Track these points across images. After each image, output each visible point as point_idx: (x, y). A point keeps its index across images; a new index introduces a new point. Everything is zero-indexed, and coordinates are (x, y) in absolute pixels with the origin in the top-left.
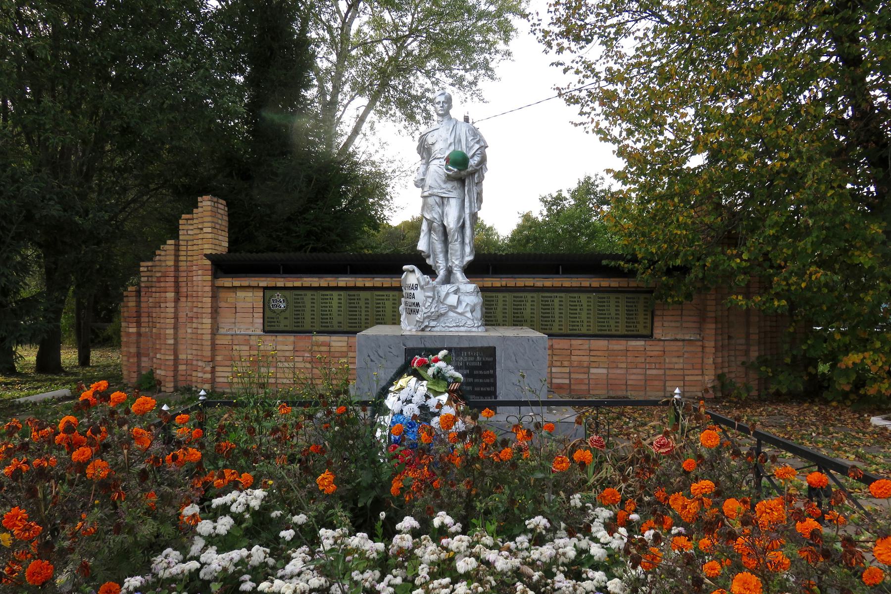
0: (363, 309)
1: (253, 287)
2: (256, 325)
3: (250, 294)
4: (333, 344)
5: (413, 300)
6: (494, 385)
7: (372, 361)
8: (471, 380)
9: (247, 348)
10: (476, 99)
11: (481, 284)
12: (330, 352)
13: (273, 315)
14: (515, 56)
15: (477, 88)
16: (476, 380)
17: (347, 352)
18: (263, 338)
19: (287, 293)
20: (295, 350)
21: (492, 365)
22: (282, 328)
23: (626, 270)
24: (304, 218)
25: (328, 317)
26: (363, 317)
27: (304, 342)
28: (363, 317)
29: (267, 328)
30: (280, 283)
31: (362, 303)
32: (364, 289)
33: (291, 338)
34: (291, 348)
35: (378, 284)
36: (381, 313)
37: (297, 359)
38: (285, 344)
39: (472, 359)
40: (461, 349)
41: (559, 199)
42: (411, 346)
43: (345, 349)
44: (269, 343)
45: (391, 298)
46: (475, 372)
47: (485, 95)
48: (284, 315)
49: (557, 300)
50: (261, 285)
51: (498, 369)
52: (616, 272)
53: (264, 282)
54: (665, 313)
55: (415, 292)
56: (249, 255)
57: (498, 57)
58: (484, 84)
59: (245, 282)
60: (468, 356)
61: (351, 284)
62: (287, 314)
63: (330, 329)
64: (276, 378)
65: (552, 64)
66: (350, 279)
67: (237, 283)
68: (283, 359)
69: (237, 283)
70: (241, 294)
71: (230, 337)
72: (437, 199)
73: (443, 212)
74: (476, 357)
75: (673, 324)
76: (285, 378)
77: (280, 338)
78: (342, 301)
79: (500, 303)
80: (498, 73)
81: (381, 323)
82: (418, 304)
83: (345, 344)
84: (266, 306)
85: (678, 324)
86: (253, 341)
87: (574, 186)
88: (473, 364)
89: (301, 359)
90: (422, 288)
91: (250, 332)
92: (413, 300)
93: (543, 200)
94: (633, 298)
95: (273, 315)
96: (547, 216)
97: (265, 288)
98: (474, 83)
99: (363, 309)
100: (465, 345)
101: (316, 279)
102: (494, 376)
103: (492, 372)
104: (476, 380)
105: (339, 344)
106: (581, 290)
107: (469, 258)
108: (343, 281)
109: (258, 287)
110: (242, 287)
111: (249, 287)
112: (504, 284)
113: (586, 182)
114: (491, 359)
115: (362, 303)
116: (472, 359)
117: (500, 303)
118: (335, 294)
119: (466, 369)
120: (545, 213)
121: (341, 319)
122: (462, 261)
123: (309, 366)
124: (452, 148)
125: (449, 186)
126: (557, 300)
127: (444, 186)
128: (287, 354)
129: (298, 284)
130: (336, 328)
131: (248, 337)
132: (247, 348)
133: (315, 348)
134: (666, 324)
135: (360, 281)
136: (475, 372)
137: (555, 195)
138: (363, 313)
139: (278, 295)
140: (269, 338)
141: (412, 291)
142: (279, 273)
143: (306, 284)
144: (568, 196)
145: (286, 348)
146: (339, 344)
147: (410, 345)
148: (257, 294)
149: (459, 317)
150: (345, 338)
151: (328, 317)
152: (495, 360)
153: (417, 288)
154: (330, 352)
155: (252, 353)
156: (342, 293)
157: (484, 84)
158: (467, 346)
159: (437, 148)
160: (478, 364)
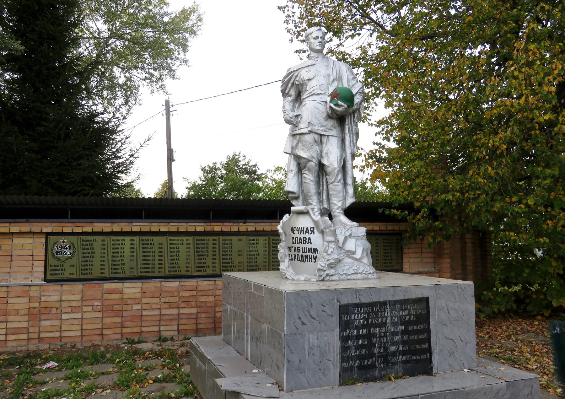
0: (157, 254)
1: (34, 233)
2: (36, 274)
3: (31, 241)
4: (126, 291)
5: (308, 246)
6: (428, 340)
7: (303, 324)
8: (406, 337)
9: (26, 300)
10: (161, 91)
11: (370, 228)
12: (122, 299)
13: (57, 263)
14: (190, 63)
15: (163, 83)
16: (412, 337)
17: (141, 299)
18: (45, 288)
19: (74, 239)
20: (83, 299)
21: (425, 318)
22: (67, 276)
23: (400, 218)
24: (79, 165)
25: (120, 263)
26: (157, 262)
27: (93, 289)
28: (157, 262)
29: (49, 277)
30: (68, 228)
31: (156, 248)
32: (160, 233)
33: (79, 287)
34: (79, 297)
35: (174, 229)
36: (175, 258)
37: (85, 309)
38: (72, 293)
39: (406, 312)
40: (395, 302)
41: (213, 169)
42: (346, 302)
43: (139, 296)
44: (53, 294)
45: (185, 242)
46: (411, 328)
47: (168, 89)
48: (69, 262)
49: (211, 242)
50: (45, 230)
51: (432, 323)
52: (392, 219)
53: (48, 227)
54: (411, 251)
55: (312, 236)
56: (35, 198)
57: (177, 63)
58: (168, 81)
59: (26, 227)
60: (402, 310)
61: (146, 229)
62: (73, 261)
63: (120, 275)
64: (61, 331)
65: (297, 51)
66: (145, 224)
67: (15, 228)
68: (69, 310)
69: (15, 228)
70: (18, 241)
71: (5, 289)
72: (317, 137)
73: (321, 151)
74: (410, 310)
75: (416, 260)
76: (72, 332)
77: (66, 287)
78: (135, 246)
79: (211, 246)
80: (177, 74)
81: (256, 270)
82: (316, 250)
83: (139, 290)
84: (49, 254)
85: (420, 260)
86: (34, 292)
87: (224, 161)
88: (408, 318)
89: (90, 309)
90: (322, 232)
91: (29, 283)
92: (308, 246)
93: (203, 170)
94: (389, 239)
95: (57, 263)
96: (204, 181)
97: (48, 234)
98: (161, 78)
99: (157, 254)
100: (400, 297)
101: (109, 224)
102: (428, 331)
103: (425, 325)
104: (412, 337)
105: (134, 290)
106: (256, 233)
107: (350, 201)
108: (137, 226)
109: (41, 233)
110: (20, 233)
111: (31, 233)
112: (383, 228)
113: (234, 158)
114: (424, 312)
115: (156, 248)
116: (406, 312)
117: (211, 246)
118: (127, 239)
119: (401, 324)
120: (203, 178)
121: (133, 264)
122: (344, 203)
123: (99, 315)
124: (335, 84)
125: (330, 123)
126: (211, 242)
127: (324, 123)
128: (74, 304)
129: (88, 229)
130: (128, 274)
131: (27, 288)
132: (26, 300)
133: (105, 296)
134: (411, 260)
135: (155, 226)
136: (411, 328)
137: (211, 165)
138: (157, 258)
139: (64, 242)
140: (54, 288)
141: (307, 236)
142: (66, 217)
143: (97, 229)
144: (220, 167)
145: (73, 298)
146: (134, 290)
147: (346, 300)
148: (37, 240)
149: (356, 263)
150: (139, 284)
151: (120, 263)
152: (428, 313)
153: (313, 232)
154: (122, 299)
155: (32, 305)
156: (135, 238)
157: (168, 81)
158: (402, 298)
159: (311, 86)
160: (413, 318)
